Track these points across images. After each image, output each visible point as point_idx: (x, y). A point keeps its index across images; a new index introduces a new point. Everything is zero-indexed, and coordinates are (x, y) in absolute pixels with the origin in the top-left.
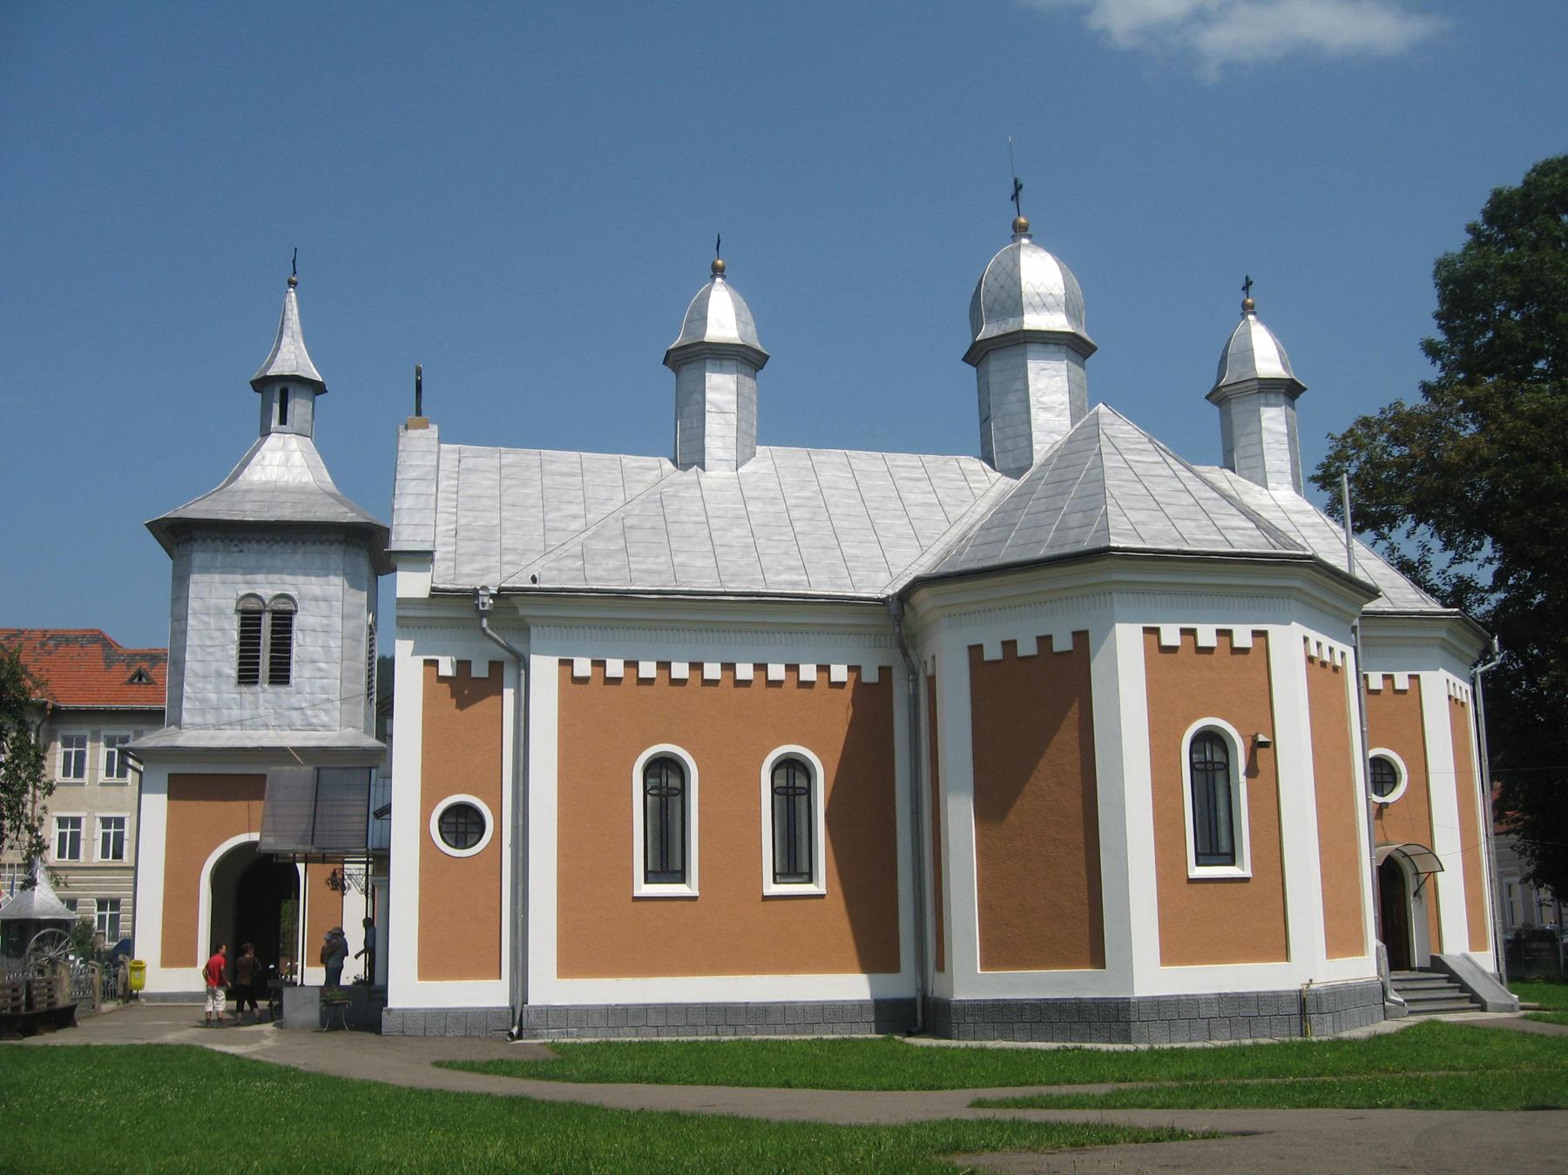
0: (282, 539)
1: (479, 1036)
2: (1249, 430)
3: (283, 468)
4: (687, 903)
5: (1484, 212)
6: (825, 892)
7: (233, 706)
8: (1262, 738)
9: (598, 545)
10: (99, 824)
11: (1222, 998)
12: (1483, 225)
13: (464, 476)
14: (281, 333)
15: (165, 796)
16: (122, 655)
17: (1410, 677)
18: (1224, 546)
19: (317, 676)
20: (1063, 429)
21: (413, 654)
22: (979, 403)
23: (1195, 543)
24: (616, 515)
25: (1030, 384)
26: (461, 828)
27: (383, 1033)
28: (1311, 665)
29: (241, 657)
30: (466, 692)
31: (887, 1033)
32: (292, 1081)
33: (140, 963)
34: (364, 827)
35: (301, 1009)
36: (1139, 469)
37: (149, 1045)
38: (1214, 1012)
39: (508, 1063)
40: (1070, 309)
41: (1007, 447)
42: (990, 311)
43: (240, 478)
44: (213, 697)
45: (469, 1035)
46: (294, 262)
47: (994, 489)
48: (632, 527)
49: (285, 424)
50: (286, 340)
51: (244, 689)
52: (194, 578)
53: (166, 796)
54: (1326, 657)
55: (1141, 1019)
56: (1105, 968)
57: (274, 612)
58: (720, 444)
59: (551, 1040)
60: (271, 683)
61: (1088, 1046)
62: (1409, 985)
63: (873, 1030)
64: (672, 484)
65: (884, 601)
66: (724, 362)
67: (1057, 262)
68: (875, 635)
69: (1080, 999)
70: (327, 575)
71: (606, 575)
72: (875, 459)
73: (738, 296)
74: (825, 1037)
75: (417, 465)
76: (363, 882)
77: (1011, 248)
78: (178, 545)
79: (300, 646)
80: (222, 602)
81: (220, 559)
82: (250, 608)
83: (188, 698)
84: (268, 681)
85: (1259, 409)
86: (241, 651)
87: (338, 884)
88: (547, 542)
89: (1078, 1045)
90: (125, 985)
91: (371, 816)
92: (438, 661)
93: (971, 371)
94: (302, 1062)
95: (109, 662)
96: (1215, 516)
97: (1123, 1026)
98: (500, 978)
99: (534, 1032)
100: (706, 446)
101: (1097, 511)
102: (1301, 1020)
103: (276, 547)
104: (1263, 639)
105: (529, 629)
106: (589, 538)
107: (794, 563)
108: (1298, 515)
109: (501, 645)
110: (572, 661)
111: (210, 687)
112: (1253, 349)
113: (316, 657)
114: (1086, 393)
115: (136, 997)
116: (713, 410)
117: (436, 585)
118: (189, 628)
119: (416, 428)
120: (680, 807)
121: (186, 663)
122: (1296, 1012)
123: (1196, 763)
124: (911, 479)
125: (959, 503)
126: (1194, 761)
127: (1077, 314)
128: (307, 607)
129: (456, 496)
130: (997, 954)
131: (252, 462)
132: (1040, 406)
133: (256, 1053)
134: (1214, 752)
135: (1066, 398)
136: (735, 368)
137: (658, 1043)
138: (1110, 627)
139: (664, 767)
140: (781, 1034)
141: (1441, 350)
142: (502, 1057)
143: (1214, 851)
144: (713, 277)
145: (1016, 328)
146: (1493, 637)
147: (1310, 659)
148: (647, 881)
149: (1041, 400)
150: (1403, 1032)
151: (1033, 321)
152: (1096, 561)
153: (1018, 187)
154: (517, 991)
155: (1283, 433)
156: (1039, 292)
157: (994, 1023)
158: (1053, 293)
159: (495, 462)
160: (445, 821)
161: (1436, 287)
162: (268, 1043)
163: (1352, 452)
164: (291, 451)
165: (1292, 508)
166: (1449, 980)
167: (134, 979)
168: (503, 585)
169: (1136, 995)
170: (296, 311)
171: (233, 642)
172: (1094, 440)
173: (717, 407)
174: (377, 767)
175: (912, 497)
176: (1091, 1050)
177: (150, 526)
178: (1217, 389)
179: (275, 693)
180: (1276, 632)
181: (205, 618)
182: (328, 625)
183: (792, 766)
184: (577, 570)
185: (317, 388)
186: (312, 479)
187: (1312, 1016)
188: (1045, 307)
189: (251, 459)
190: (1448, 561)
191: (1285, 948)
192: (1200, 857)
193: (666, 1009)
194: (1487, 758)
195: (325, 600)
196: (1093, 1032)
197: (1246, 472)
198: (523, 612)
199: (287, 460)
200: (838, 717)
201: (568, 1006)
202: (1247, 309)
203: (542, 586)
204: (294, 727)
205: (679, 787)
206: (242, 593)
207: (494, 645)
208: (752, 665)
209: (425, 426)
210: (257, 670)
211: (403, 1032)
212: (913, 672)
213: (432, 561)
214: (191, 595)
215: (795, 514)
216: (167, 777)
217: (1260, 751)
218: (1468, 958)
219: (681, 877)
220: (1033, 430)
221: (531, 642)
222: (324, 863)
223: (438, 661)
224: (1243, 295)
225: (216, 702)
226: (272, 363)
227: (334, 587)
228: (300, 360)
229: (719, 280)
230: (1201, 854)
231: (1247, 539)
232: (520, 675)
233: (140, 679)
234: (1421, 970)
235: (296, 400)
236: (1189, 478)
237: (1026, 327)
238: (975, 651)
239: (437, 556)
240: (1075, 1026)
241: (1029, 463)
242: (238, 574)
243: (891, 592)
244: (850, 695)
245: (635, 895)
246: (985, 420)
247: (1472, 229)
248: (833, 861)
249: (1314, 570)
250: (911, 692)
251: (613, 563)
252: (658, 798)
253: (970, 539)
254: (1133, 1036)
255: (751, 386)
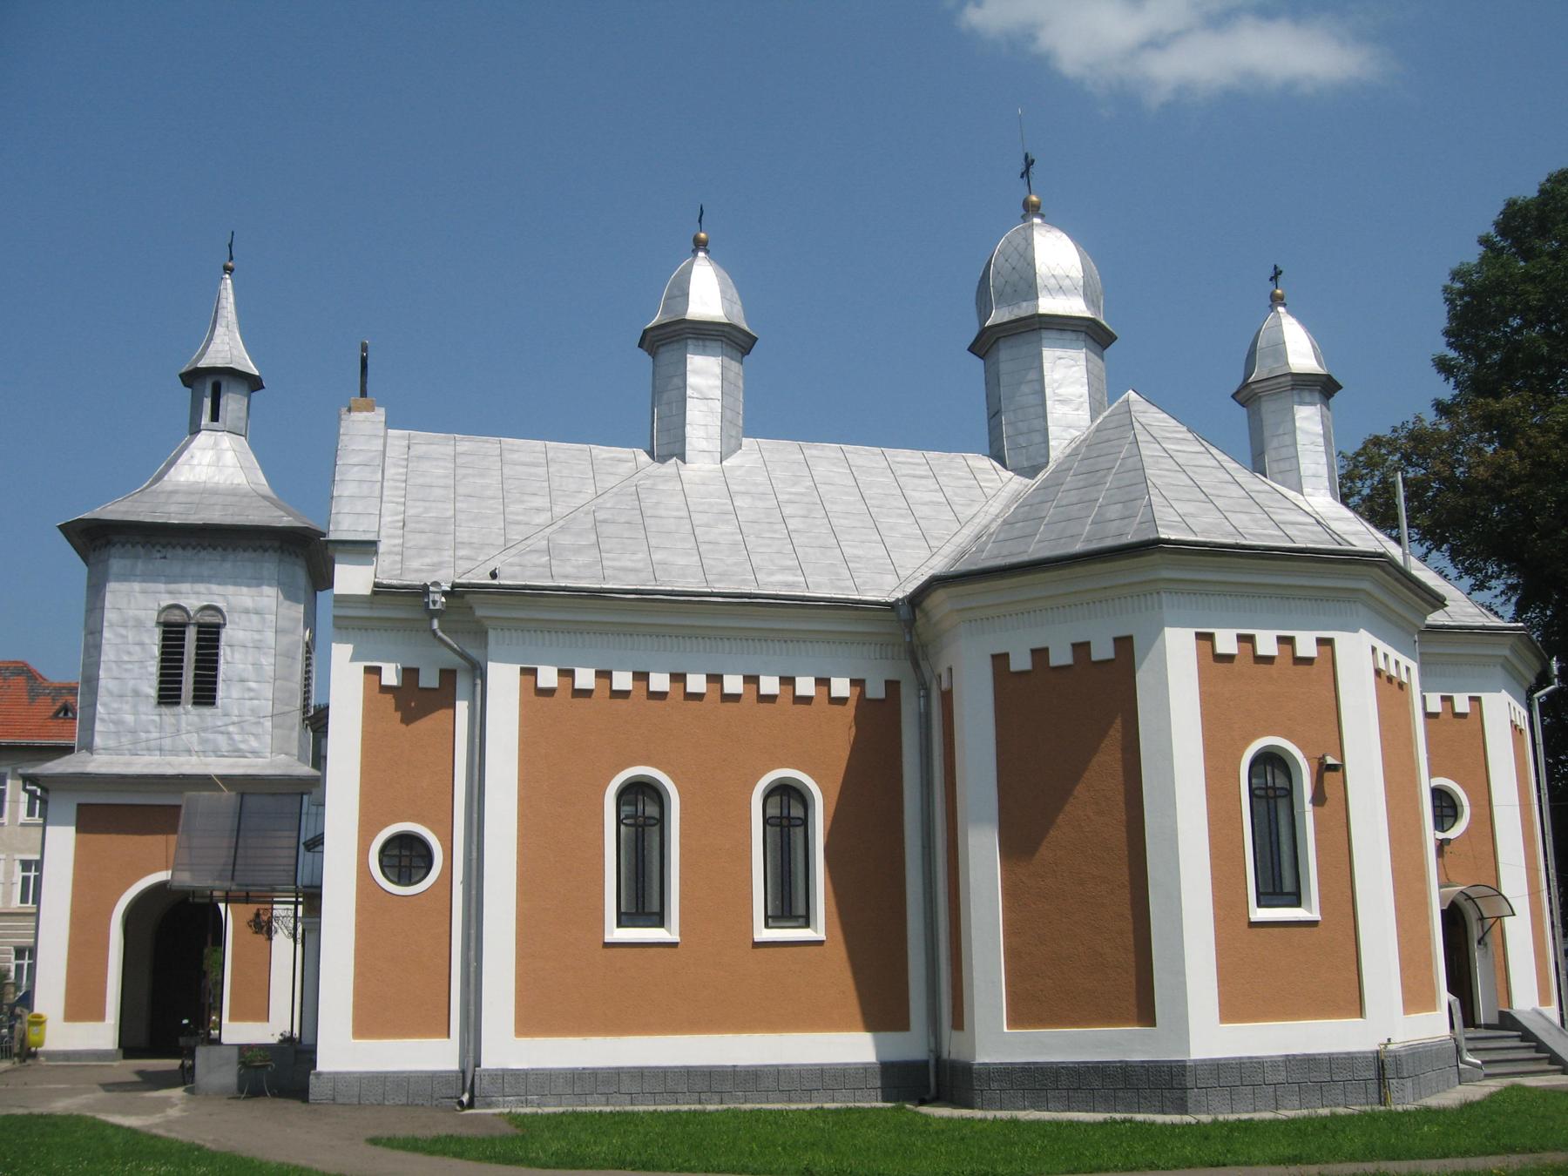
0: (210, 545)
1: (423, 1105)
2: (1281, 431)
3: (213, 468)
4: (667, 950)
5: (1496, 224)
6: (824, 938)
7: (152, 728)
8: (1330, 760)
9: (566, 540)
10: (18, 867)
11: (1290, 1060)
12: (1496, 237)
13: (415, 464)
14: (215, 322)
15: (73, 829)
16: (47, 688)
17: (1471, 698)
18: (1287, 542)
19: (246, 696)
20: (1082, 423)
21: (354, 659)
22: (987, 396)
23: (1251, 537)
24: (586, 508)
25: (1045, 373)
26: (405, 862)
27: (310, 1101)
28: (1378, 679)
29: (162, 675)
30: (413, 704)
31: (898, 1101)
32: (194, 1164)
33: (39, 1016)
34: (293, 861)
35: (216, 1071)
36: (1181, 459)
37: (31, 1116)
38: (1281, 1078)
39: (459, 1140)
40: (1089, 293)
41: (1020, 444)
42: (1000, 295)
43: (166, 478)
44: (129, 718)
45: (412, 1103)
46: (230, 246)
47: (1007, 489)
48: (605, 521)
49: (217, 421)
50: (220, 330)
51: (164, 710)
52: (112, 586)
53: (74, 828)
54: (1393, 672)
55: (1199, 1085)
56: (1155, 1026)
57: (200, 625)
58: (702, 434)
59: (507, 1110)
60: (195, 703)
61: (1139, 1117)
62: (1480, 1045)
63: (879, 1098)
64: (648, 477)
65: (892, 606)
66: (708, 343)
67: (1076, 246)
68: (882, 645)
69: (1126, 1062)
70: (259, 585)
71: (576, 572)
72: (874, 454)
73: (722, 271)
74: (826, 1106)
75: (361, 450)
76: (291, 925)
77: (1023, 228)
78: (94, 550)
79: (227, 663)
80: (142, 614)
81: (140, 565)
82: (173, 621)
83: (103, 720)
84: (192, 701)
85: (1293, 407)
86: (162, 668)
87: (263, 927)
88: (508, 536)
89: (1128, 1116)
90: (23, 1040)
91: (302, 847)
92: (380, 668)
93: (977, 363)
94: (211, 1137)
95: (34, 694)
96: (1270, 509)
97: (1178, 1093)
98: (449, 1036)
99: (488, 1100)
100: (687, 435)
101: (1139, 502)
102: (1379, 1086)
103: (203, 554)
104: (1329, 648)
105: (486, 633)
106: (553, 532)
107: (790, 563)
108: (1337, 522)
109: (454, 650)
110: (536, 670)
111: (126, 707)
112: (1285, 343)
113: (245, 675)
114: (1105, 387)
115: (34, 1055)
116: (695, 395)
117: (380, 581)
118: (103, 641)
119: (360, 410)
120: (658, 839)
121: (100, 680)
122: (1373, 1077)
123: (1257, 789)
124: (915, 476)
125: (969, 502)
126: (1254, 786)
127: (1095, 299)
128: (237, 620)
129: (404, 485)
130: (1026, 1010)
131: (179, 461)
132: (1056, 398)
133: (157, 1125)
134: (1276, 776)
135: (1085, 390)
136: (720, 350)
137: (633, 1113)
138: (1159, 631)
139: (640, 793)
140: (773, 1102)
141: (1454, 366)
142: (450, 1133)
143: (1278, 890)
144: (695, 252)
145: (1029, 313)
146: (1551, 659)
147: (1378, 672)
148: (619, 925)
149: (1058, 391)
150: (1492, 1097)
151: (1048, 305)
152: (1141, 556)
153: (1029, 163)
154: (468, 1052)
155: (1318, 434)
156: (1056, 273)
157: (1023, 1090)
158: (1070, 275)
159: (449, 450)
160: (386, 853)
161: (1445, 303)
162: (173, 1113)
163: (1365, 471)
164: (221, 449)
165: (1331, 515)
166: (1522, 1039)
167: (32, 1037)
168: (458, 581)
169: (1193, 1057)
170: (231, 299)
171: (153, 658)
172: (1126, 428)
173: (700, 392)
174: (310, 793)
175: (916, 495)
176: (1144, 1123)
177: (61, 528)
178: (1245, 385)
179: (199, 715)
180: (1342, 640)
181: (123, 631)
182: (260, 641)
183: (786, 792)
184: (543, 566)
185: (252, 384)
186: (245, 482)
187: (1390, 1081)
188: (1061, 290)
189: (179, 457)
190: (1468, 588)
191: (1358, 1000)
192: (1262, 897)
193: (640, 1074)
194: (1546, 791)
195: (257, 613)
196: (1142, 1100)
197: (1279, 477)
198: (479, 613)
199: (219, 459)
200: (840, 735)
201: (528, 1070)
202: (1276, 300)
203: (502, 582)
204: (219, 753)
205: (657, 816)
206: (164, 604)
207: (447, 651)
208: (742, 677)
209: (370, 408)
210: (180, 689)
211: (333, 1100)
212: (924, 687)
213: (376, 553)
214: (107, 604)
215: (787, 511)
216: (75, 807)
217: (1328, 775)
218: (1541, 1014)
219: (659, 920)
220: (1049, 424)
221: (489, 647)
222: (247, 903)
223: (380, 668)
224: (1271, 286)
225: (133, 724)
226: (204, 354)
227: (266, 599)
228: (235, 352)
229: (701, 254)
230: (1262, 894)
231: (1308, 535)
232: (475, 685)
233: (66, 714)
234: (1488, 1027)
235: (230, 395)
236: (1237, 469)
237: (1042, 311)
238: (1000, 660)
239: (382, 548)
240: (1120, 1094)
241: (1044, 460)
242: (159, 582)
243: (900, 595)
244: (852, 712)
245: (606, 941)
246: (994, 415)
247: (1485, 241)
248: (832, 902)
249: (1383, 569)
250: (922, 710)
251: (583, 559)
252: (634, 829)
253: (992, 534)
254: (1189, 1105)
255: (737, 371)
